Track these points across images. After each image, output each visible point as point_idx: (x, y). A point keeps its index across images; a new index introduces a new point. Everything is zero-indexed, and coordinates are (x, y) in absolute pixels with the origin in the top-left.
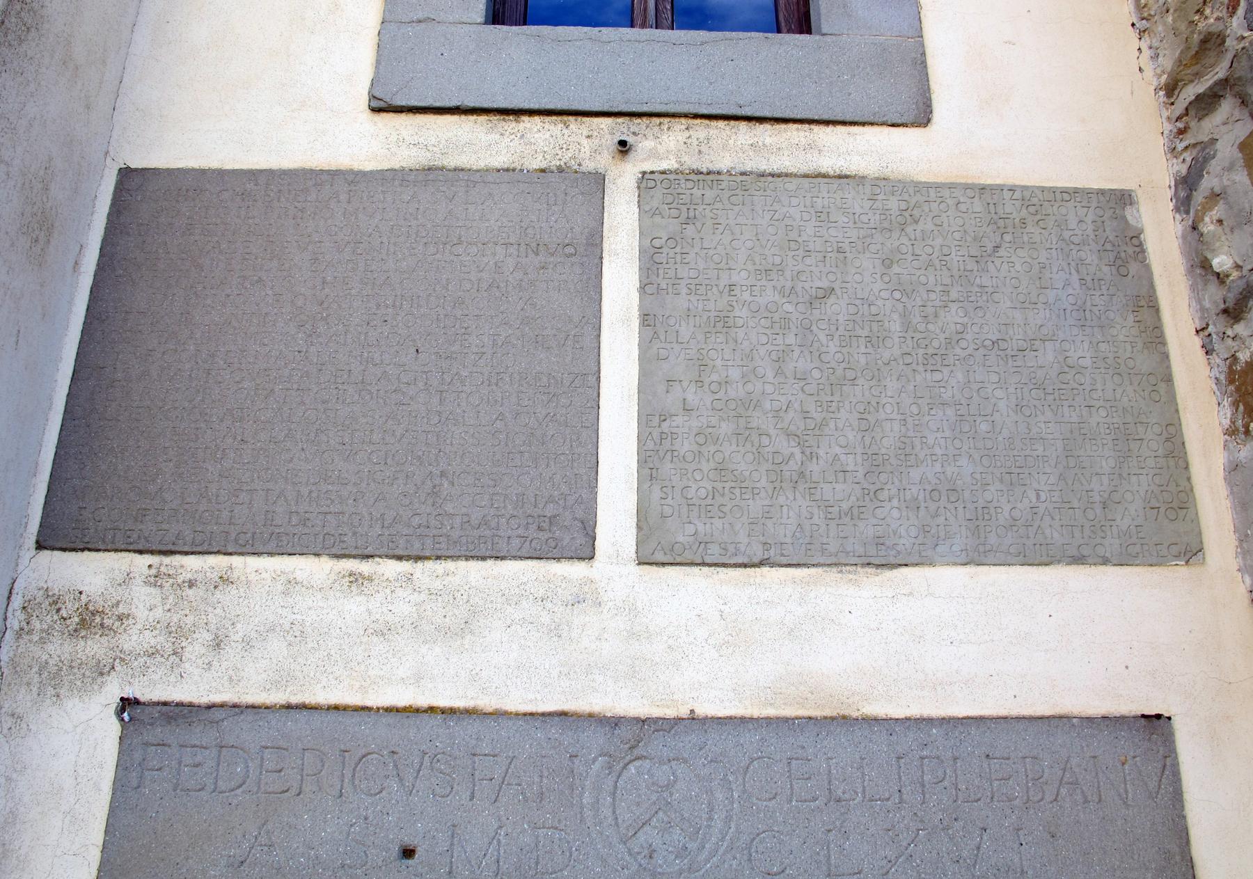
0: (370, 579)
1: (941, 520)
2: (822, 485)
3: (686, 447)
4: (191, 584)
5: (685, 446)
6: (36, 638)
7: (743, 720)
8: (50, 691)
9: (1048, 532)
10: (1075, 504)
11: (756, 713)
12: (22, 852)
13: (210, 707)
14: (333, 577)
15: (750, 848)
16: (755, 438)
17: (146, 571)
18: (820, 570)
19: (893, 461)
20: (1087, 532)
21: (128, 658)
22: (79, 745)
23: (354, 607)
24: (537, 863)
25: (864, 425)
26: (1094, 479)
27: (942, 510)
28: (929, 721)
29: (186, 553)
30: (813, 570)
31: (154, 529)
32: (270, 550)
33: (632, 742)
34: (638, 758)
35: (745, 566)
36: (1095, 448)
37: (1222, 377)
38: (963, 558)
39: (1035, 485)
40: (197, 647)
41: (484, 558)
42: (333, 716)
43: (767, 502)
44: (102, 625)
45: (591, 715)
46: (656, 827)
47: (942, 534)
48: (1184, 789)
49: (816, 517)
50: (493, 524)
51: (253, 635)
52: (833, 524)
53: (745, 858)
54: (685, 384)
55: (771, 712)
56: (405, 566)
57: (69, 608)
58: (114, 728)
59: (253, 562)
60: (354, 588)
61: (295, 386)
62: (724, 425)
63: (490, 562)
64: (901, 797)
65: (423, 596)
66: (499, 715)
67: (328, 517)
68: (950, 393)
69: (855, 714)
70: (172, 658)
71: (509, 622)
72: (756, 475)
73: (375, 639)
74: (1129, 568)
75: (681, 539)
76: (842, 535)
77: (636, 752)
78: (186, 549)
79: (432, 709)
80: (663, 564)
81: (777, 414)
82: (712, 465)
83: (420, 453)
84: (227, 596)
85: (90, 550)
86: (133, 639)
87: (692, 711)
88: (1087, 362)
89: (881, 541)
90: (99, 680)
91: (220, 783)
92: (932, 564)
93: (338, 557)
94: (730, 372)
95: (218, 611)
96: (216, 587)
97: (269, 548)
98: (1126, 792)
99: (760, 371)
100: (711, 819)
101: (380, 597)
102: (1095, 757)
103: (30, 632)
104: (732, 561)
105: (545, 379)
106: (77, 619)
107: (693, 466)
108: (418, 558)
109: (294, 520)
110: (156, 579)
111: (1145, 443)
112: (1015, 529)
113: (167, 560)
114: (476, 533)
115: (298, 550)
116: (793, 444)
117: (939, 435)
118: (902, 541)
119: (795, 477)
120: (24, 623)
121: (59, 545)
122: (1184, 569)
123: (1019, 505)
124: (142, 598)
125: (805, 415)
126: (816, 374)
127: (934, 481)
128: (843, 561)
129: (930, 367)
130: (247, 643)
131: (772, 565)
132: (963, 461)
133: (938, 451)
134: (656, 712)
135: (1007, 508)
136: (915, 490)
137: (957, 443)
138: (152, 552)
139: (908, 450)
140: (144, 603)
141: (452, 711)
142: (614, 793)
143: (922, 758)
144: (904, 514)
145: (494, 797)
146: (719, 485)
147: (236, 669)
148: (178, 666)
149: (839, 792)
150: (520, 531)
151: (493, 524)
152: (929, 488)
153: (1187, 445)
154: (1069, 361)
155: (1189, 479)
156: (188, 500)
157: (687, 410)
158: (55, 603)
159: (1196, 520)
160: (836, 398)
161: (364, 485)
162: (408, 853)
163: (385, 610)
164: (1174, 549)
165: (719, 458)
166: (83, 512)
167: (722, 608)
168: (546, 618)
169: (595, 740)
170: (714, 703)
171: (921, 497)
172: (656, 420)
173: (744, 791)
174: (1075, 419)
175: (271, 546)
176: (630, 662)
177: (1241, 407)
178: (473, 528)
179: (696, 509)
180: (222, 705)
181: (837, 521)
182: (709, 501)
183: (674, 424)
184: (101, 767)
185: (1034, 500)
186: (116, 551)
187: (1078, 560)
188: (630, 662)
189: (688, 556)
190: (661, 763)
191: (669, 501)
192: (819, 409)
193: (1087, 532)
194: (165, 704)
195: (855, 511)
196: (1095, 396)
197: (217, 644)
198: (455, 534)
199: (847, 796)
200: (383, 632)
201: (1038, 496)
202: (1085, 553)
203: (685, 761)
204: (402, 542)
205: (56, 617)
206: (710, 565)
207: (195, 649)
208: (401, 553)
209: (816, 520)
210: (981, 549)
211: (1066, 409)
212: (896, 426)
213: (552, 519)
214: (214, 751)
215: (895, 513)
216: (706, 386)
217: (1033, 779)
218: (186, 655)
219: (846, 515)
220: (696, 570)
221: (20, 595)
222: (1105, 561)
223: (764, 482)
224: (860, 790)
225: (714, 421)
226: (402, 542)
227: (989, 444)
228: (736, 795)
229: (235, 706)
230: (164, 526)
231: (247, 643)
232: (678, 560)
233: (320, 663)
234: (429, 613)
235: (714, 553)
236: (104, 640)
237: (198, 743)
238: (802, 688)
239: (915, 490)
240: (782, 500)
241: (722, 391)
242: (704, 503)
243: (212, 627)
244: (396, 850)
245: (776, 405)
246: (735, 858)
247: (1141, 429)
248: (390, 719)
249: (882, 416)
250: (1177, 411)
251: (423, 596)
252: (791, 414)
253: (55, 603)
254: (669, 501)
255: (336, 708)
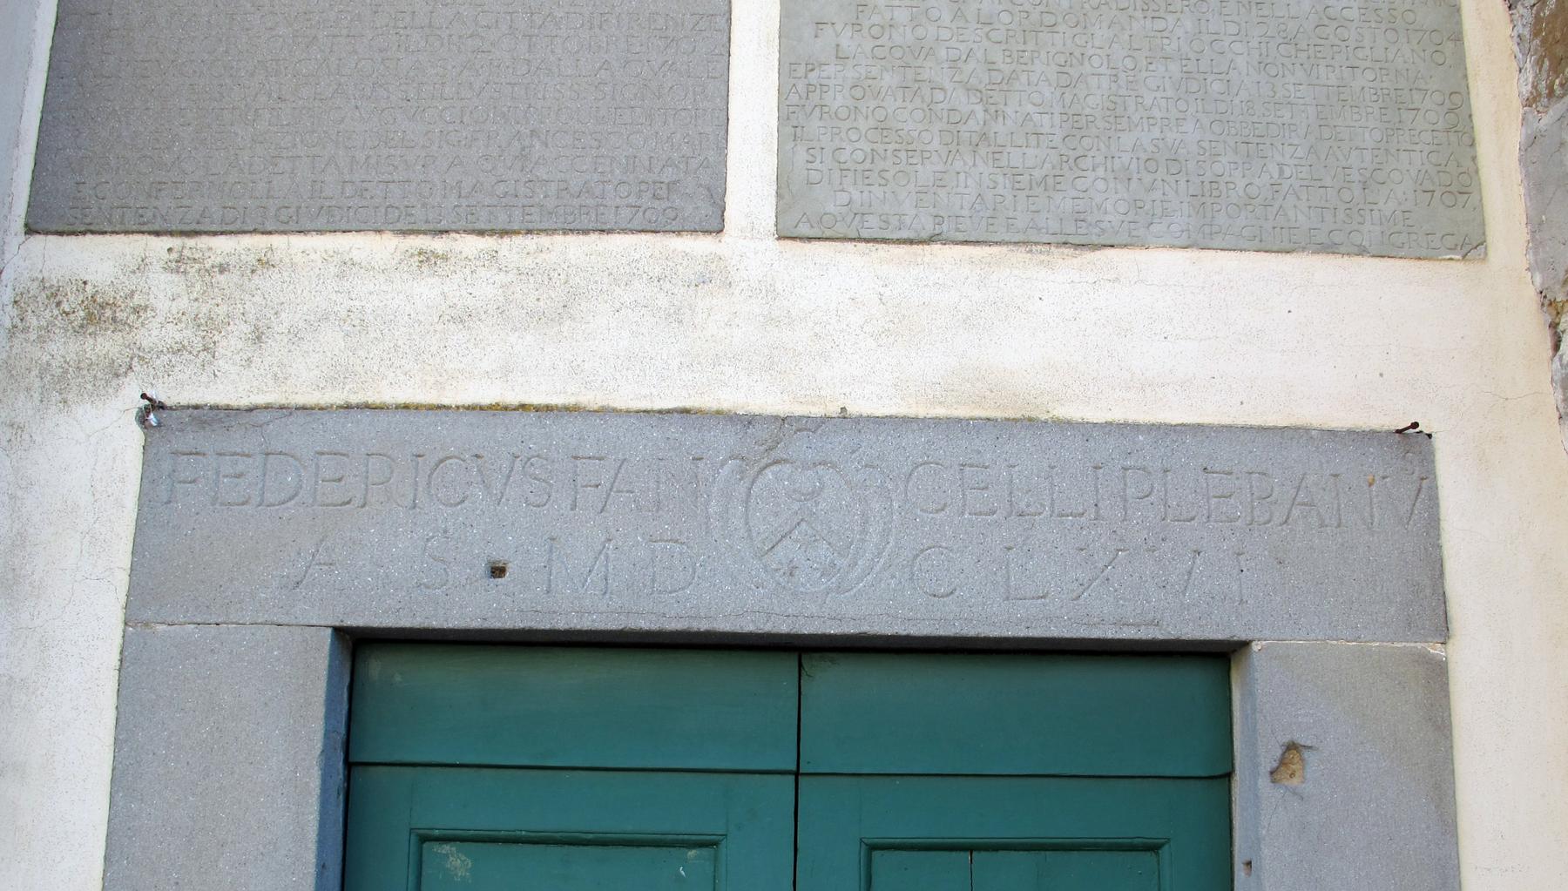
0: (445, 258)
1: (1157, 195)
2: (1009, 149)
3: (839, 101)
4: (223, 269)
5: (838, 100)
6: (33, 336)
7: (906, 421)
8: (55, 397)
9: (1291, 213)
10: (1328, 182)
11: (921, 412)
12: (36, 577)
13: (250, 410)
14: (398, 256)
15: (912, 566)
16: (926, 91)
17: (166, 256)
18: (1004, 249)
19: (1100, 124)
20: (1341, 215)
21: (148, 356)
22: (95, 456)
23: (427, 290)
24: (653, 581)
25: (1064, 80)
26: (1354, 153)
27: (1159, 183)
28: (1136, 427)
29: (215, 233)
30: (995, 249)
31: (173, 206)
32: (319, 227)
33: (770, 443)
34: (776, 462)
35: (911, 242)
36: (1356, 117)
37: (1526, 32)
38: (1183, 241)
39: (1279, 158)
40: (233, 341)
41: (586, 232)
42: (400, 416)
43: (940, 167)
44: (114, 319)
45: (718, 412)
46: (797, 541)
47: (1158, 211)
48: (1442, 517)
49: (1000, 186)
50: (598, 192)
51: (301, 324)
52: (1022, 195)
53: (907, 576)
54: (839, 27)
55: (941, 412)
56: (488, 243)
57: (71, 301)
58: (136, 435)
59: (298, 242)
60: (425, 268)
61: (344, 32)
62: (887, 76)
63: (594, 237)
64: (1097, 512)
65: (511, 276)
66: (605, 412)
67: (391, 186)
68: (1174, 45)
69: (1043, 417)
70: (202, 355)
71: (617, 305)
72: (926, 136)
73: (452, 326)
74: (1391, 261)
75: (831, 208)
76: (1033, 208)
77: (776, 454)
78: (214, 228)
79: (523, 407)
80: (810, 239)
81: (954, 63)
82: (872, 122)
83: (505, 109)
84: (267, 282)
85: (93, 232)
86: (152, 335)
87: (843, 409)
88: (1353, 13)
89: (1082, 216)
90: (115, 382)
91: (267, 495)
92: (1145, 246)
93: (405, 233)
94: (896, 13)
95: (257, 299)
96: (253, 272)
97: (319, 224)
98: (1372, 516)
99: (934, 14)
100: (864, 531)
101: (457, 278)
102: (1336, 476)
103: (25, 330)
104: (895, 236)
105: (661, 21)
106: (82, 314)
107: (848, 124)
108: (504, 233)
109: (349, 190)
110: (178, 265)
111: (1421, 113)
112: (1250, 208)
113: (191, 242)
114: (576, 202)
115: (354, 226)
116: (973, 99)
117: (1158, 95)
118: (1108, 217)
119: (975, 139)
120: (17, 321)
121: (54, 228)
122: (1460, 266)
123: (1257, 181)
124: (162, 287)
125: (990, 65)
126: (1006, 18)
127: (1151, 148)
128: (1033, 239)
129: (1150, 14)
130: (295, 335)
131: (945, 242)
132: (1189, 126)
133: (1156, 113)
134: (799, 410)
135: (1241, 183)
136: (1126, 158)
137: (1182, 105)
138: (171, 233)
139: (1120, 111)
140: (165, 293)
141: (549, 408)
142: (747, 502)
143: (1125, 469)
144: (1112, 185)
145: (600, 506)
146: (880, 148)
147: (281, 365)
148: (210, 363)
149: (1023, 505)
150: (632, 200)
151: (598, 192)
152: (1144, 156)
153: (1475, 118)
154: (1330, 11)
155: (1474, 158)
156: (214, 171)
157: (841, 58)
158: (54, 295)
159: (1479, 208)
160: (1031, 46)
161: (435, 148)
162: (497, 571)
163: (464, 293)
164: (1450, 241)
165: (880, 114)
166: (81, 187)
167: (882, 290)
168: (663, 301)
169: (725, 440)
170: (872, 400)
171: (1134, 166)
172: (801, 70)
173: (906, 501)
174: (1333, 81)
175: (321, 222)
176: (766, 351)
177: (1547, 63)
178: (572, 196)
179: (850, 174)
180: (267, 407)
181: (1027, 192)
182: (867, 165)
183: (824, 74)
184: (123, 480)
185: (1276, 175)
186: (126, 233)
187: (1328, 248)
188: (766, 351)
189: (841, 230)
190: (805, 467)
191: (817, 165)
192: (1008, 60)
193: (1341, 215)
194: (196, 407)
195: (1050, 181)
196: (1360, 55)
197: (258, 338)
198: (550, 204)
199: (1032, 510)
200: (463, 318)
201: (1281, 172)
202: (1337, 240)
203: (834, 466)
204: (484, 213)
205: (56, 312)
206: (867, 241)
207: (231, 343)
208: (483, 227)
209: (1000, 190)
210: (1207, 230)
211: (1322, 69)
212: (1105, 81)
213: (671, 186)
214: (260, 459)
215: (1101, 185)
216: (865, 30)
217: (1259, 498)
218: (220, 351)
219: (1039, 185)
220: (850, 246)
221: (9, 289)
222: (1362, 251)
223: (936, 144)
224: (1047, 503)
225: (875, 72)
226: (484, 213)
227: (1222, 107)
228: (895, 505)
229: (282, 408)
230: (185, 202)
231: (295, 335)
232: (828, 233)
233: (385, 356)
234: (518, 296)
235: (873, 226)
236: (118, 336)
237: (239, 450)
238: (979, 385)
239: (1126, 158)
240: (958, 165)
241: (886, 36)
242: (860, 167)
243: (251, 317)
244: (482, 568)
245: (953, 54)
246: (893, 577)
247: (1417, 96)
248: (472, 417)
249: (1087, 68)
250: (1466, 76)
251: (511, 276)
252: (972, 65)
253: (54, 295)
254: (817, 165)
255: (406, 407)
